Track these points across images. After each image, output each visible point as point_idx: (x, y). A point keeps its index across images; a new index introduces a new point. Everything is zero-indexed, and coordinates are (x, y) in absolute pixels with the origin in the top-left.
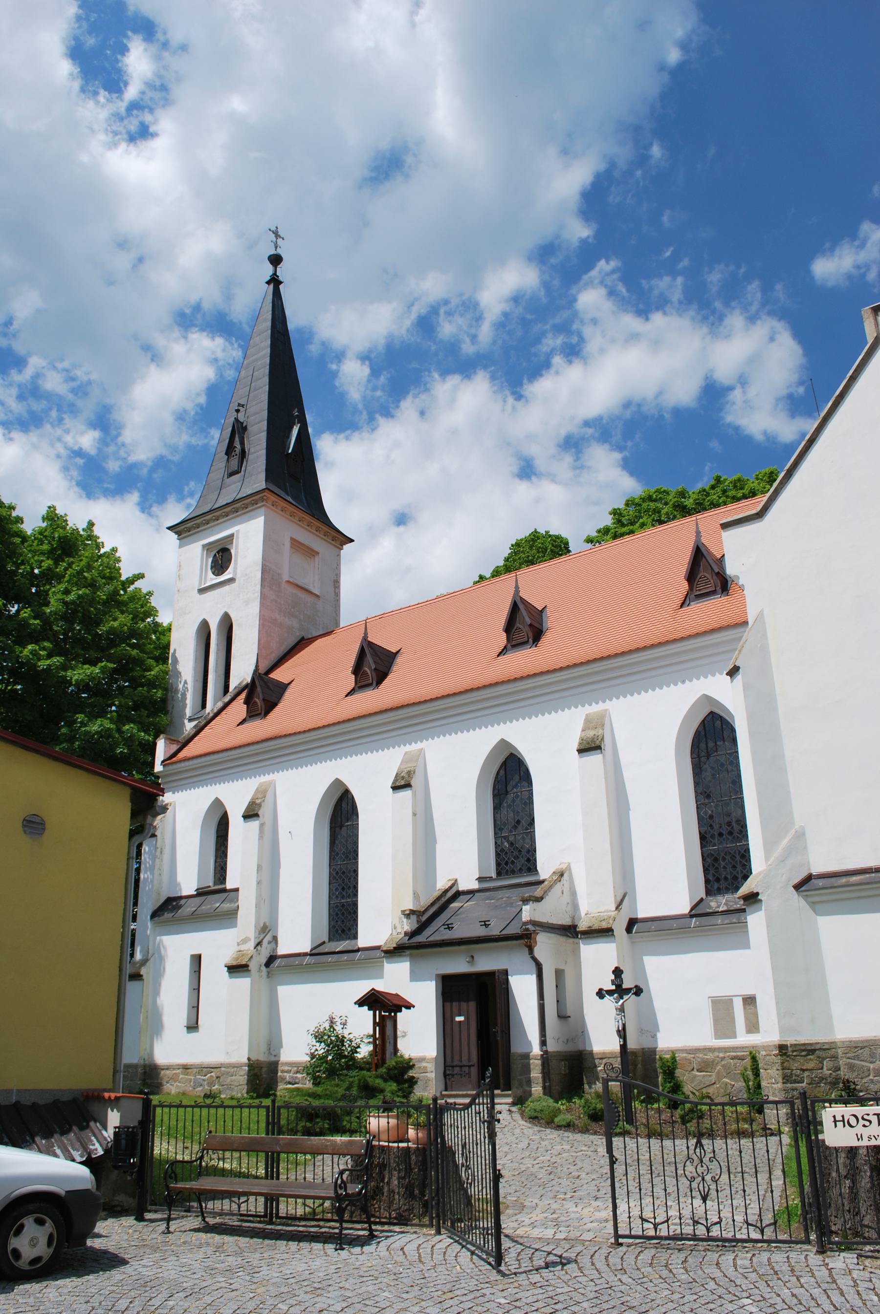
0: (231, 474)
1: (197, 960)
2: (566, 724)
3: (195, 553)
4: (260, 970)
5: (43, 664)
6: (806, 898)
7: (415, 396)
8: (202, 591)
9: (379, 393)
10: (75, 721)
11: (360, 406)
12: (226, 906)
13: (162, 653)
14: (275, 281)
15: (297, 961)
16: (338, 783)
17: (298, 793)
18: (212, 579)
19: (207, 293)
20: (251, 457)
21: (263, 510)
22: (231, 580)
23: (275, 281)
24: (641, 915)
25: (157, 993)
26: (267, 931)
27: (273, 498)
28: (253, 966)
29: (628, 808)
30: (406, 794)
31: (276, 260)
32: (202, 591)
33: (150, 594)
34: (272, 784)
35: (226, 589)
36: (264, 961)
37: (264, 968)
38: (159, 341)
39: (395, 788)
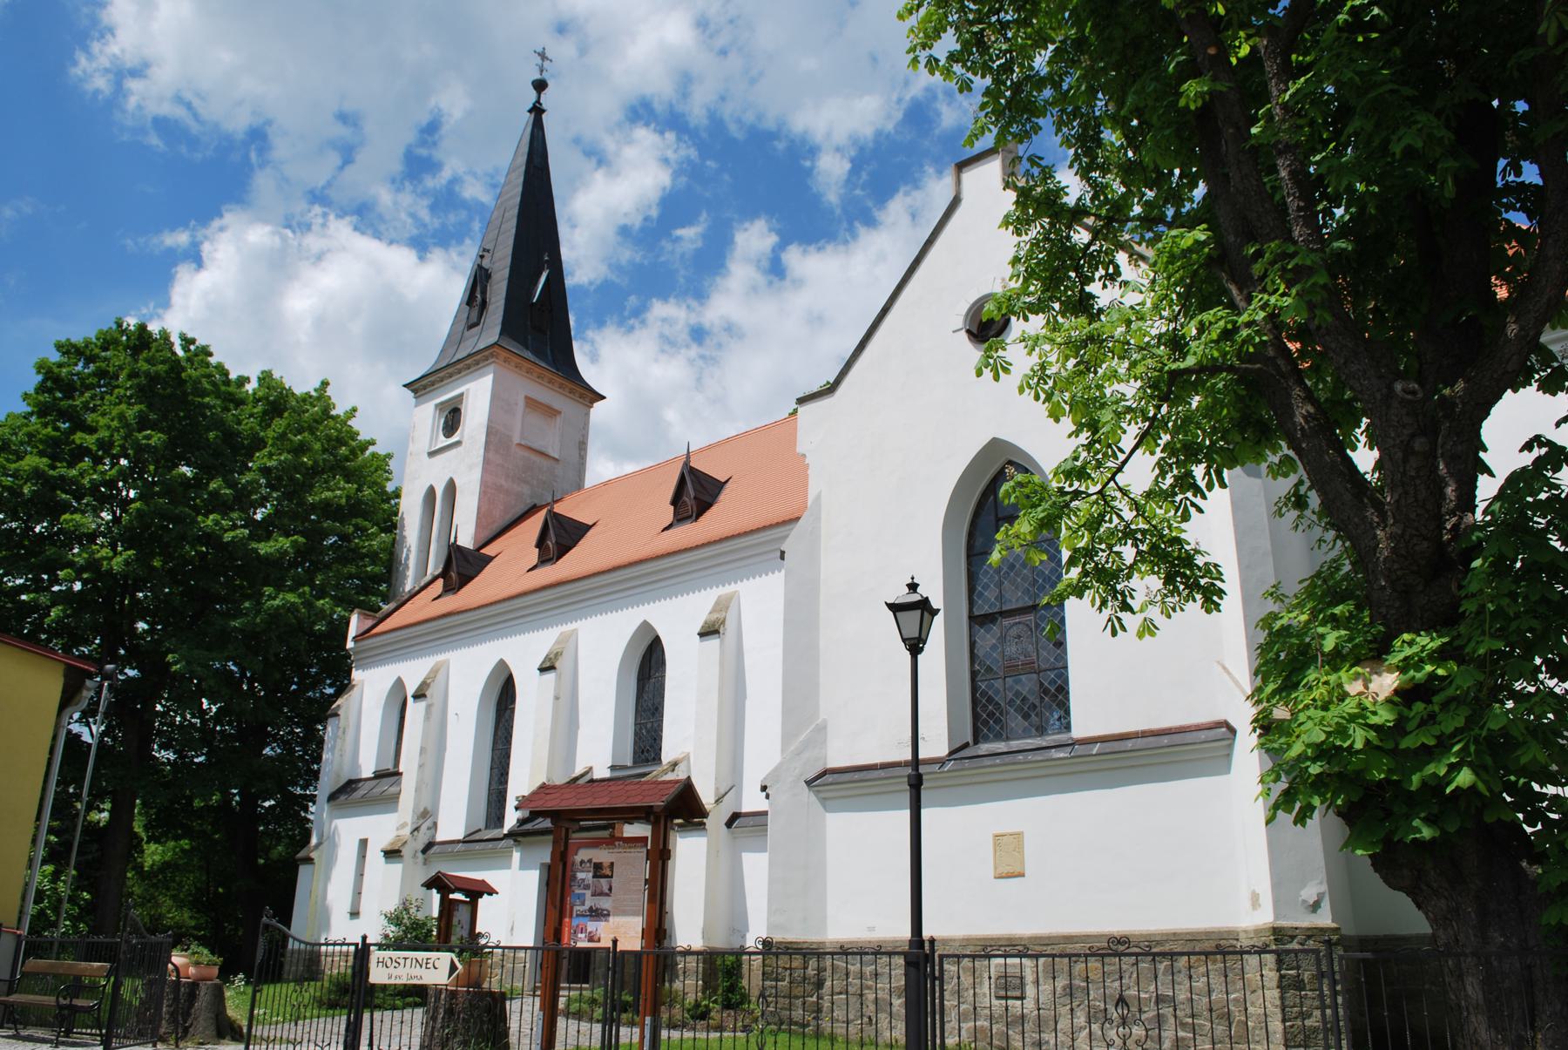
0: (470, 327)
1: (364, 843)
2: (696, 605)
3: (426, 415)
4: (415, 856)
5: (228, 537)
6: (817, 793)
7: (907, 194)
8: (432, 454)
9: (858, 192)
10: (262, 595)
11: (838, 211)
12: (393, 790)
13: (390, 523)
14: (537, 111)
15: (449, 848)
16: (646, 627)
17: (466, 671)
18: (443, 441)
19: (660, 87)
20: (491, 308)
21: (492, 367)
22: (458, 443)
23: (537, 111)
24: (744, 810)
25: (328, 878)
26: (427, 816)
27: (504, 354)
28: (406, 852)
29: (744, 697)
30: (551, 676)
31: (540, 86)
32: (432, 454)
33: (389, 456)
34: (446, 663)
35: (453, 452)
36: (421, 847)
37: (420, 855)
38: (609, 144)
39: (702, 635)
